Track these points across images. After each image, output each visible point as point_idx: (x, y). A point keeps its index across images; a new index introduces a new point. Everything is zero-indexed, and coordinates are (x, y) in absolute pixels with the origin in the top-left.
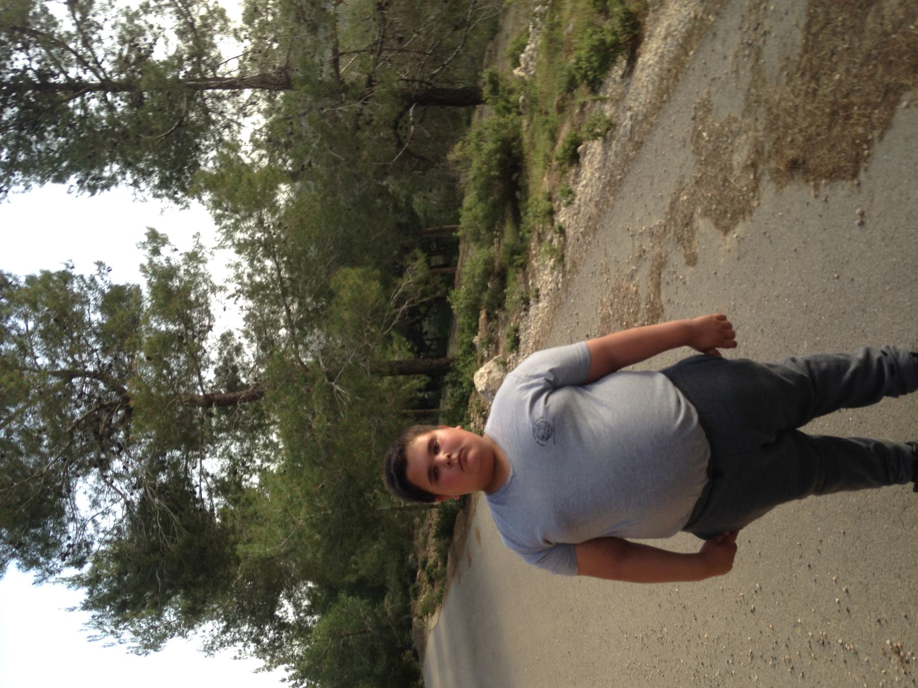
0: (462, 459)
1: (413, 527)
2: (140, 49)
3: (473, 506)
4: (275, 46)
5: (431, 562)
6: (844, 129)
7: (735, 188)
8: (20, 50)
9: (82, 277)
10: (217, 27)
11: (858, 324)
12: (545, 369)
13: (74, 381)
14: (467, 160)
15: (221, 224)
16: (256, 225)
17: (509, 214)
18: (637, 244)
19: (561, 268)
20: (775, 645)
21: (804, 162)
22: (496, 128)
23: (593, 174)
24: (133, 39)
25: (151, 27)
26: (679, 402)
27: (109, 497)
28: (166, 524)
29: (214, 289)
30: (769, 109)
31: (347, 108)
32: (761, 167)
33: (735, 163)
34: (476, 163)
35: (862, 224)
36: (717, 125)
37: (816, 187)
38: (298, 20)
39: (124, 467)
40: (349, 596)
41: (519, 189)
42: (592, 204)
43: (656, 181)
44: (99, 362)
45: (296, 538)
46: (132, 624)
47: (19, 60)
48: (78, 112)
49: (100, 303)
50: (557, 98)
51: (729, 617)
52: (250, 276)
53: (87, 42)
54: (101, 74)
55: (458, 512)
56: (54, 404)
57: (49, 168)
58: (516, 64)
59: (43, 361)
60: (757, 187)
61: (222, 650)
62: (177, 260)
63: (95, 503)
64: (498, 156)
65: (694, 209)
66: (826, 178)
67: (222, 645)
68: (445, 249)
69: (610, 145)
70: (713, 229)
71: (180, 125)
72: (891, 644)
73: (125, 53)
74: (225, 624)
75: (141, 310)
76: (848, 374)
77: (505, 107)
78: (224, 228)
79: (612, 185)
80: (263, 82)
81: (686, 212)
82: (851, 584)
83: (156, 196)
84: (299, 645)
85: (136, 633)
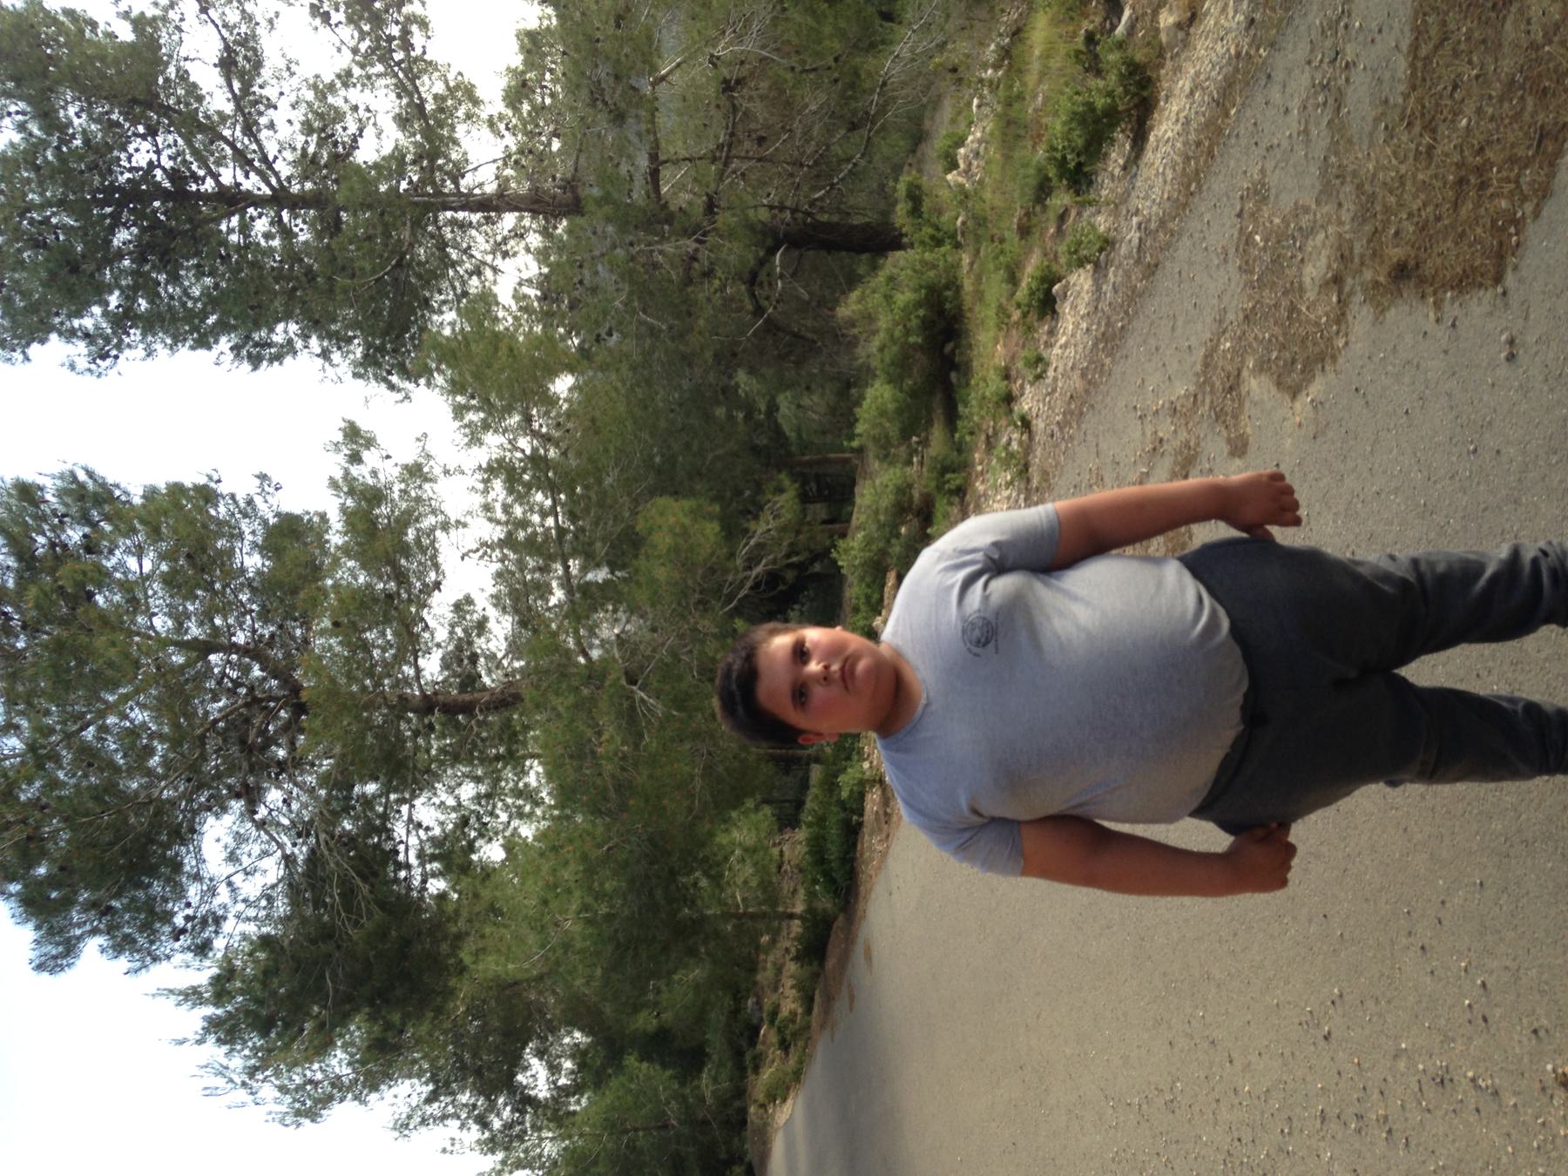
0: (847, 673)
1: (758, 948)
2: (335, 144)
3: (861, 905)
4: (556, 145)
5: (784, 1012)
6: (1477, 205)
7: (1308, 321)
8: (144, 137)
9: (233, 497)
10: (461, 113)
11: (1508, 526)
12: (986, 540)
13: (212, 658)
14: (870, 318)
15: (462, 419)
16: (520, 426)
17: (938, 398)
18: (1149, 430)
19: (1023, 486)
20: (1361, 1094)
21: (1417, 266)
22: (918, 267)
23: (1076, 325)
24: (325, 126)
25: (355, 108)
26: (1200, 600)
27: (256, 849)
28: (348, 894)
29: (445, 526)
30: (1360, 187)
31: (673, 248)
32: (1349, 281)
33: (1307, 280)
34: (883, 322)
35: (1511, 357)
36: (1277, 221)
37: (1438, 305)
38: (593, 103)
39: (285, 801)
40: (642, 1061)
41: (954, 366)
42: (1076, 375)
43: (1179, 323)
44: (254, 631)
45: (560, 952)
46: (277, 1074)
47: (141, 153)
48: (234, 238)
49: (259, 540)
50: (1019, 212)
51: (1287, 1052)
52: (506, 508)
53: (250, 129)
54: (274, 181)
55: (836, 918)
56: (176, 694)
57: (183, 326)
58: (953, 165)
59: (162, 623)
60: (1343, 314)
61: (423, 1129)
62: (389, 472)
63: (232, 857)
64: (921, 312)
65: (1243, 362)
66: (1452, 288)
67: (424, 1122)
68: (831, 490)
69: (1106, 276)
70: (1274, 390)
71: (399, 265)
72: (1554, 1071)
73: (311, 149)
74: (431, 1087)
75: (325, 553)
76: (1482, 582)
77: (932, 237)
78: (466, 426)
79: (1109, 340)
80: (537, 201)
81: (1230, 368)
82: (1492, 972)
83: (356, 375)
84: (552, 1139)
85: (283, 1089)
